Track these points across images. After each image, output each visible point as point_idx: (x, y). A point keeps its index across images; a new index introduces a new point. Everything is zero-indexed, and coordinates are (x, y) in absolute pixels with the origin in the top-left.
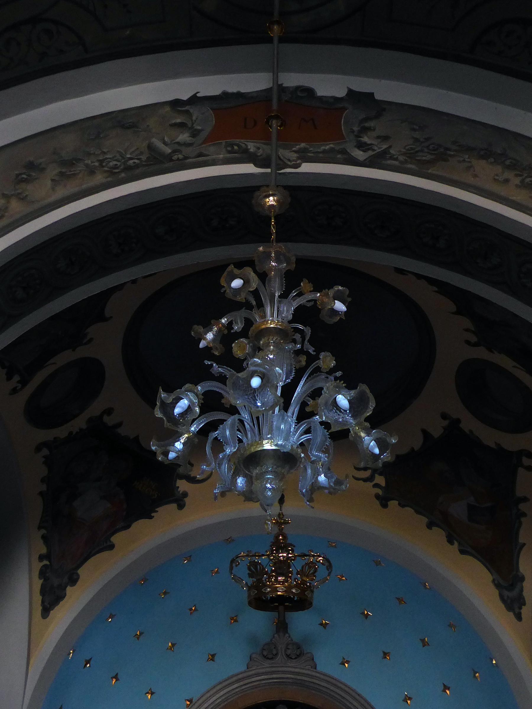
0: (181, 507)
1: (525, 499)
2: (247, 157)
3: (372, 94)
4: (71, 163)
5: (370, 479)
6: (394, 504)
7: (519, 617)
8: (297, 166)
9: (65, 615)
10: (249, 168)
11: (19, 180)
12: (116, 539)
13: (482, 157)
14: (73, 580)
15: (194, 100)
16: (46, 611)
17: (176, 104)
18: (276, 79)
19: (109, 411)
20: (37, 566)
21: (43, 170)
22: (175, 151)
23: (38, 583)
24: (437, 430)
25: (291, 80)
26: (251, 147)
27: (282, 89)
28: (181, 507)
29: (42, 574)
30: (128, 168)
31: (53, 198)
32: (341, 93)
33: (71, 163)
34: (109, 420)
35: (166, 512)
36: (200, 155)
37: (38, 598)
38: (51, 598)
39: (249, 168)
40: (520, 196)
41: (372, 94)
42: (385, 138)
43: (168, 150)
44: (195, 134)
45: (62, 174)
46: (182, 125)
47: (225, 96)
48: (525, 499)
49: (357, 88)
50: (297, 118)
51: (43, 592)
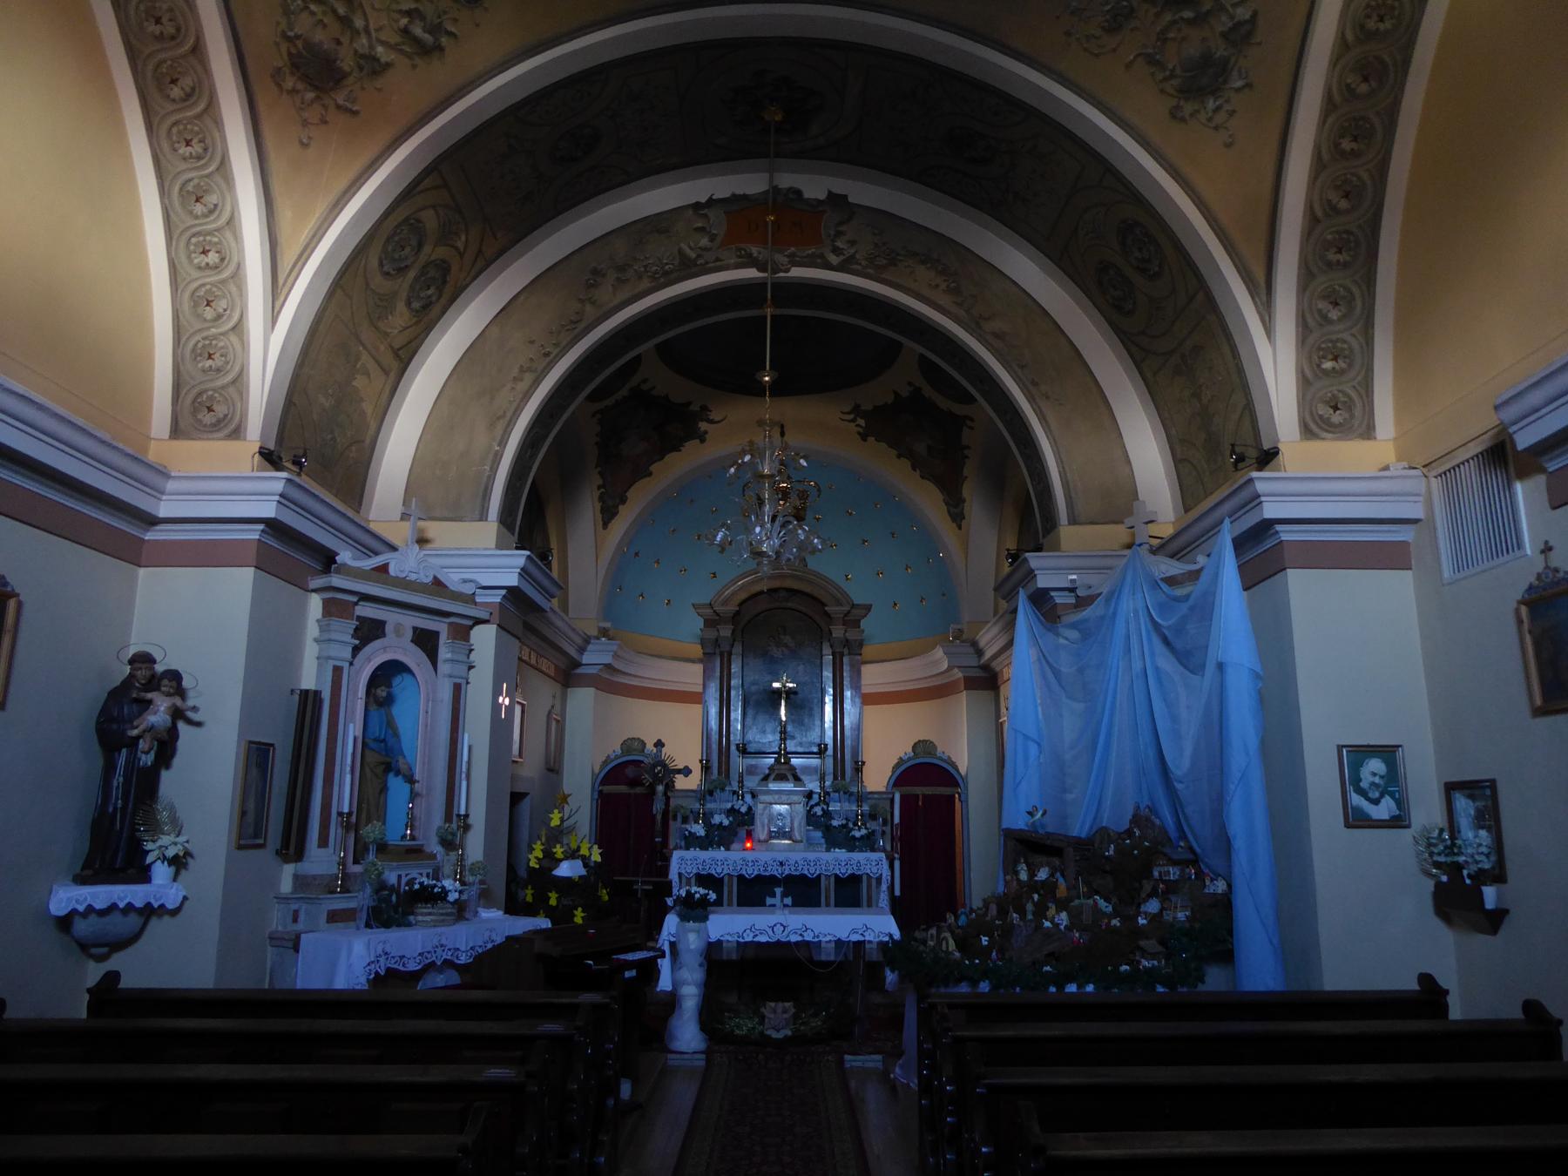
0: (703, 441)
1: (968, 447)
2: (751, 262)
3: (845, 197)
4: (622, 269)
5: (853, 421)
6: (871, 439)
7: (960, 527)
8: (787, 271)
9: (620, 526)
10: (751, 273)
11: (591, 286)
12: (652, 468)
13: (923, 262)
14: (623, 501)
15: (711, 202)
16: (605, 525)
17: (697, 206)
18: (771, 179)
19: (645, 381)
20: (597, 494)
21: (604, 275)
22: (699, 256)
23: (598, 506)
24: (905, 392)
25: (786, 180)
26: (755, 251)
27: (776, 190)
28: (703, 441)
29: (601, 499)
30: (666, 273)
31: (616, 302)
32: (822, 196)
33: (622, 269)
34: (645, 387)
35: (691, 446)
36: (718, 260)
37: (599, 516)
38: (608, 515)
39: (751, 273)
40: (945, 300)
41: (845, 197)
42: (852, 243)
43: (693, 255)
44: (712, 240)
45: (618, 279)
46: (701, 230)
47: (735, 198)
48: (968, 447)
49: (837, 190)
50: (788, 221)
51: (603, 511)
